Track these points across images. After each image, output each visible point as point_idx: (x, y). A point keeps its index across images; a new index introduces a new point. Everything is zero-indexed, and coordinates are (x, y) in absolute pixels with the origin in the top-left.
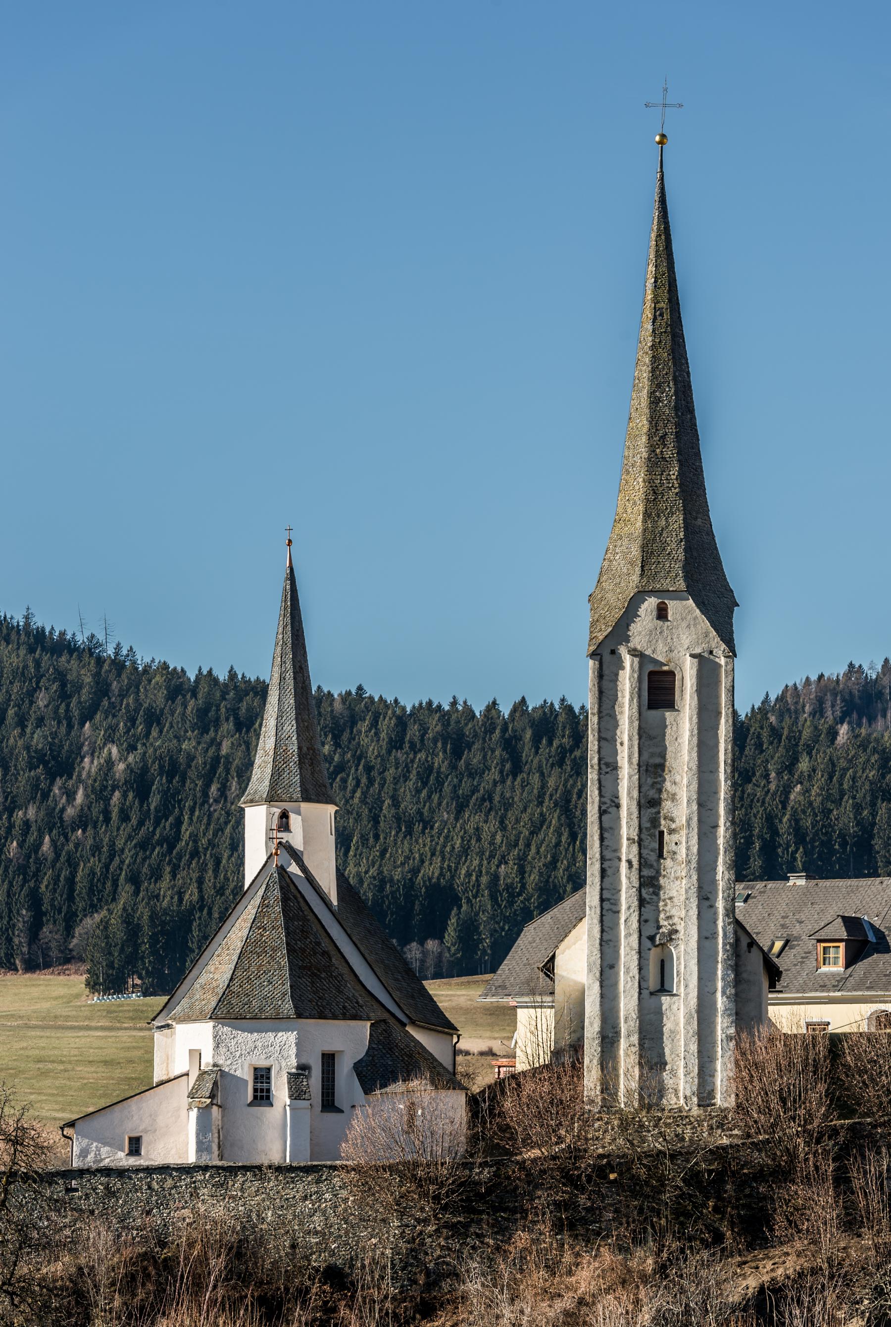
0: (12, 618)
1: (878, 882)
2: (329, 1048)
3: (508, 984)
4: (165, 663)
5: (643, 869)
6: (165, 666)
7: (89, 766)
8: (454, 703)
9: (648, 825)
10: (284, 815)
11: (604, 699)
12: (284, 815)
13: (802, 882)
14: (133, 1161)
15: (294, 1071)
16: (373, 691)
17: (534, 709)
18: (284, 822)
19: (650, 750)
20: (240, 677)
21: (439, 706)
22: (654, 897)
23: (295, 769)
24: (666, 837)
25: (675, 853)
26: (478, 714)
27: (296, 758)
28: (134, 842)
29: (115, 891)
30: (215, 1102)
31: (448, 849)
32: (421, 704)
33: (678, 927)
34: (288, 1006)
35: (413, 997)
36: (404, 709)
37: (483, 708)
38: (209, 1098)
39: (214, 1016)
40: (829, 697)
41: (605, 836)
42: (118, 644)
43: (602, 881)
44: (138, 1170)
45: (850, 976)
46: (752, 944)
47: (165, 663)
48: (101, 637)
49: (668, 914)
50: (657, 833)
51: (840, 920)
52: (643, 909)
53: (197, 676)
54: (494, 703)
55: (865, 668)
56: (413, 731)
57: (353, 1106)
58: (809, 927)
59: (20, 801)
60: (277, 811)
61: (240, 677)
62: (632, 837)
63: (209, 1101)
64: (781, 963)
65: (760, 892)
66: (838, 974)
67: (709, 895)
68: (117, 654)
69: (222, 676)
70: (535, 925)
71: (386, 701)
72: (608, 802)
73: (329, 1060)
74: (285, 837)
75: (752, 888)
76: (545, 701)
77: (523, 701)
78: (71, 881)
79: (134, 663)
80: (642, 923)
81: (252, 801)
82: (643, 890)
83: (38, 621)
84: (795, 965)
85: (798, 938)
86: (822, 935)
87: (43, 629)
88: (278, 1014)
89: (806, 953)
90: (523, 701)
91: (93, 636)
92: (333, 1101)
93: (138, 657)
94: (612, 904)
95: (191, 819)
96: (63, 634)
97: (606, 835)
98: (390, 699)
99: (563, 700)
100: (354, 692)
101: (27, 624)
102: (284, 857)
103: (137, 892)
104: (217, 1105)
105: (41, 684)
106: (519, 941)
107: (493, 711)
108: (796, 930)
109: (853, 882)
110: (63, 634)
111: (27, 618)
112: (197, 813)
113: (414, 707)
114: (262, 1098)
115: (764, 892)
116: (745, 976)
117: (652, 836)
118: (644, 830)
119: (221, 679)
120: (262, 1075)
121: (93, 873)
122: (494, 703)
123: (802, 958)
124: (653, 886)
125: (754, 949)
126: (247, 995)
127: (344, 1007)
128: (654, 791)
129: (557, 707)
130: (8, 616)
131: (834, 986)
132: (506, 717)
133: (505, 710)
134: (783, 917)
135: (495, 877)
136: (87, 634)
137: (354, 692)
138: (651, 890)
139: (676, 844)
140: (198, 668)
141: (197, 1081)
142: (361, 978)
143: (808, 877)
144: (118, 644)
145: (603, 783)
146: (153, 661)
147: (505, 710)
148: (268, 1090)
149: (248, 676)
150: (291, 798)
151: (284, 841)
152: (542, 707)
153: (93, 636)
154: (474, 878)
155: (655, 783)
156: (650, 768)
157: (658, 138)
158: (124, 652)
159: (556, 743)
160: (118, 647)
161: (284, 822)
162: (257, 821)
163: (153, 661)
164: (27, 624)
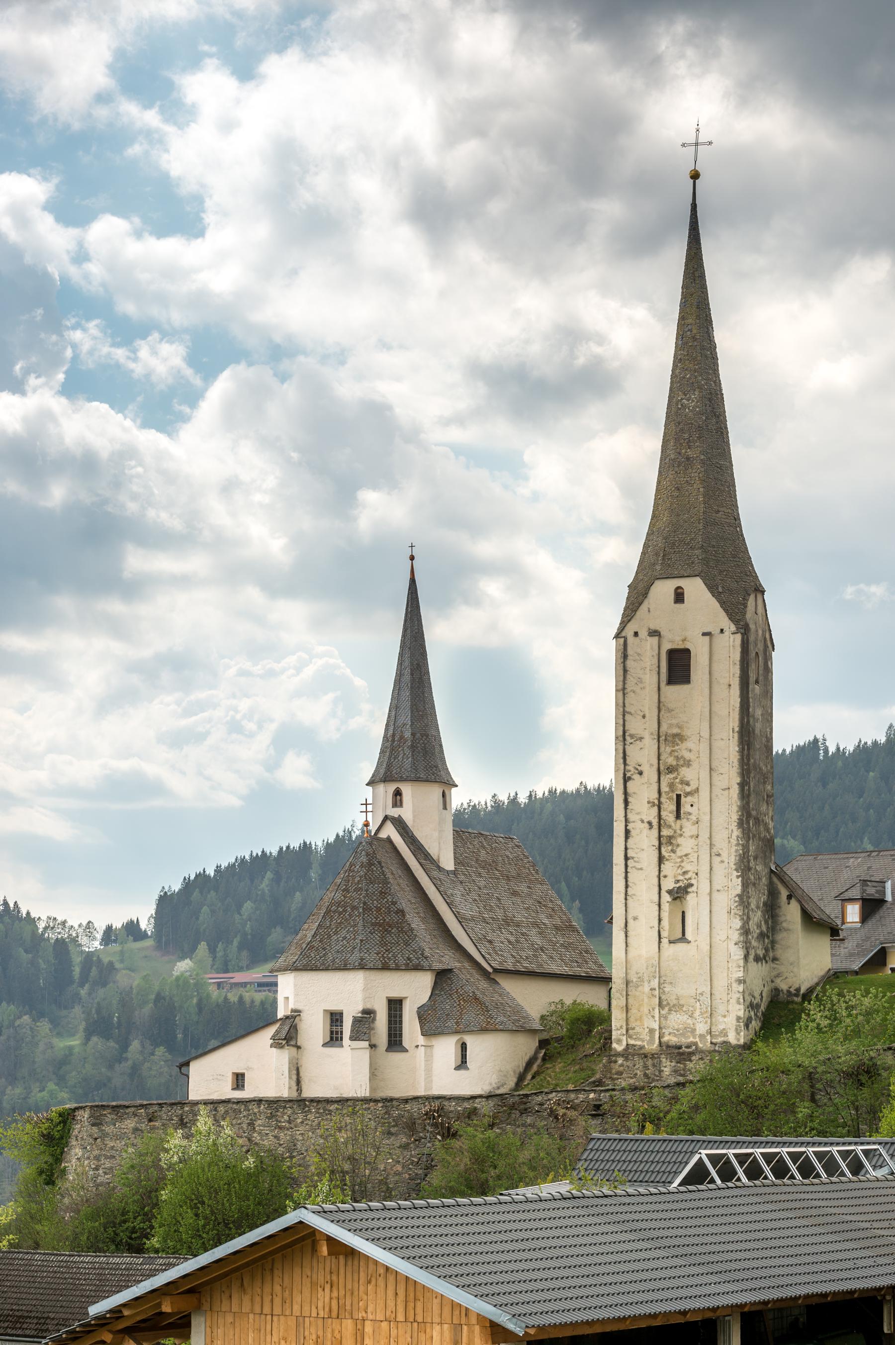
2: (395, 994)
5: (663, 830)
9: (667, 789)
10: (398, 793)
11: (628, 676)
12: (398, 793)
15: (360, 1015)
22: (672, 854)
24: (683, 799)
33: (693, 881)
38: (285, 1039)
43: (626, 841)
49: (684, 870)
50: (675, 797)
52: (662, 866)
57: (417, 1046)
59: (646, 978)
72: (632, 769)
73: (395, 1005)
80: (662, 878)
86: (847, 895)
88: (345, 965)
92: (401, 1041)
97: (630, 799)
114: (337, 1039)
117: (670, 799)
118: (663, 795)
126: (324, 949)
127: (409, 959)
139: (692, 805)
145: (628, 753)
150: (401, 777)
155: (673, 751)
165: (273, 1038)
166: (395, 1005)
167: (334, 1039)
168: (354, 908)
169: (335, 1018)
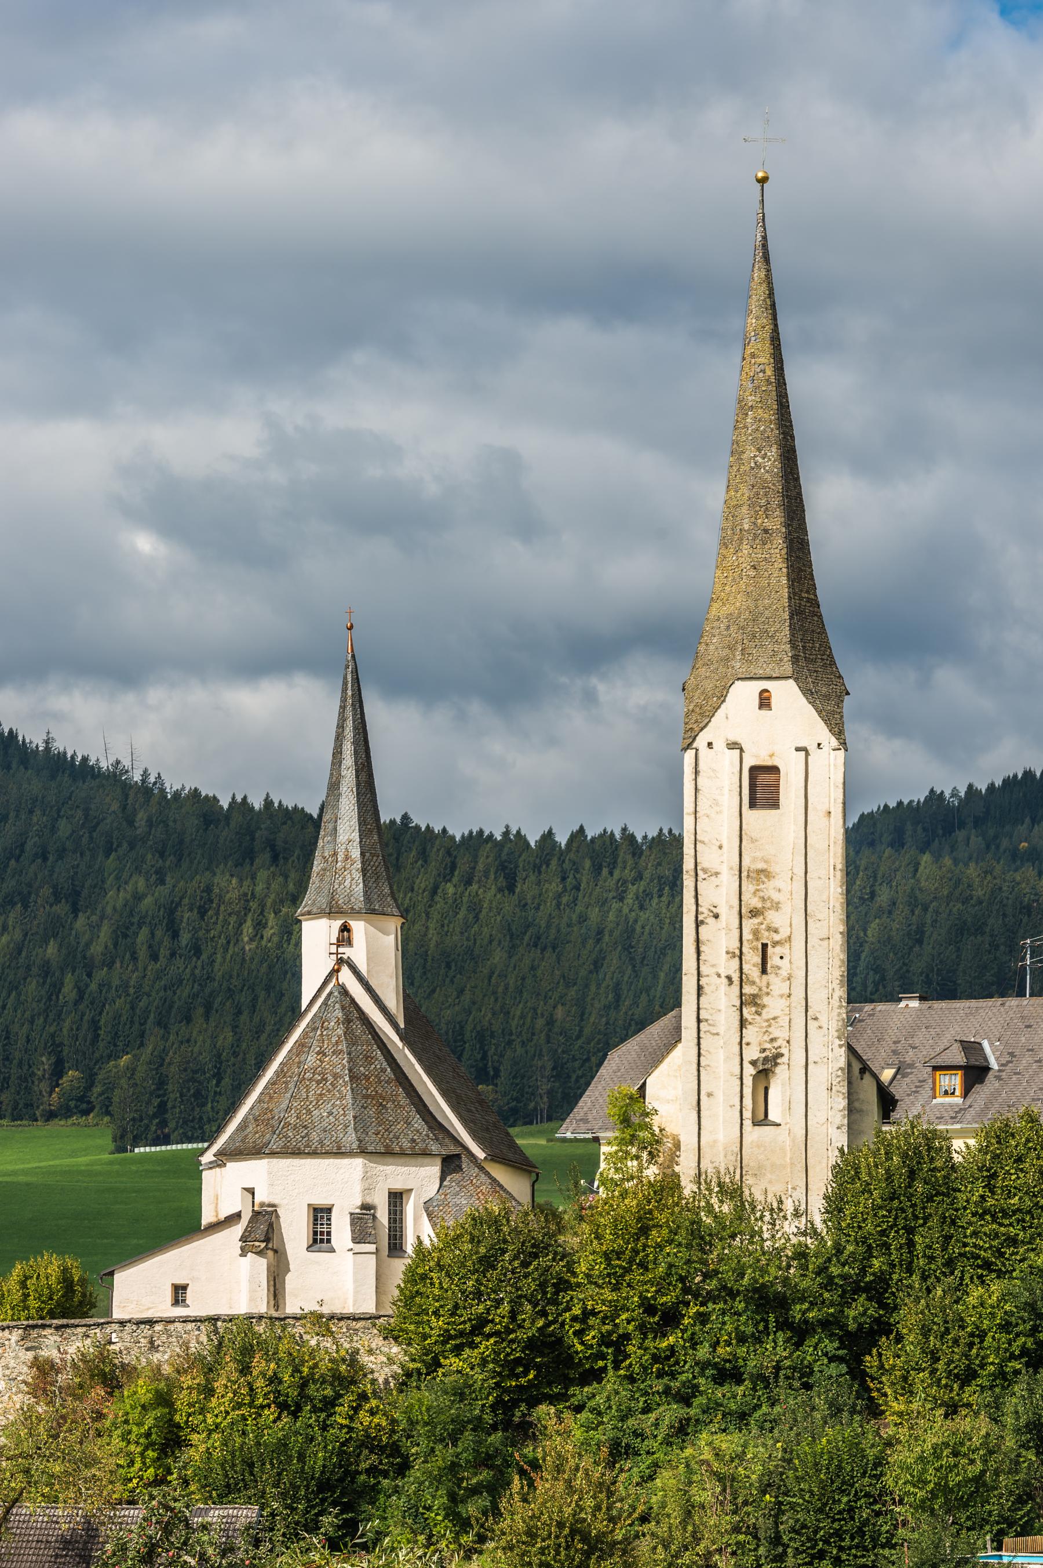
0: (31, 742)
1: (999, 1003)
3: (590, 1117)
4: (196, 789)
6: (196, 793)
7: (114, 899)
8: (506, 834)
9: (751, 937)
10: (345, 928)
12: (345, 928)
13: (915, 1004)
14: (180, 1312)
16: (420, 821)
17: (593, 839)
18: (345, 936)
19: (753, 855)
20: (276, 805)
21: (491, 836)
22: (757, 1017)
23: (358, 876)
24: (770, 950)
25: (779, 968)
26: (533, 844)
27: (358, 865)
28: (163, 983)
29: (142, 1035)
30: (270, 1246)
31: (500, 989)
32: (471, 832)
34: (350, 1139)
35: (487, 1129)
36: (453, 838)
37: (538, 838)
39: (363, 1152)
40: (909, 827)
41: (701, 949)
42: (146, 771)
44: (185, 1320)
45: (970, 1107)
46: (865, 1069)
47: (196, 789)
48: (126, 763)
49: (771, 1036)
50: (760, 946)
51: (957, 1045)
52: (744, 1030)
53: (230, 804)
54: (550, 832)
55: (947, 795)
56: (463, 865)
58: (926, 1052)
60: (338, 924)
61: (276, 805)
62: (731, 950)
63: (263, 1245)
64: (897, 1091)
65: (870, 1015)
66: (957, 1105)
67: (818, 1015)
68: (143, 781)
69: (257, 803)
70: (619, 1052)
71: (433, 831)
73: (397, 1198)
74: (347, 952)
75: (860, 1011)
76: (605, 830)
77: (582, 829)
78: (95, 1025)
79: (162, 790)
81: (309, 913)
82: (744, 1009)
83: (58, 746)
84: (909, 1095)
85: (911, 1066)
86: (939, 1061)
87: (65, 753)
89: (920, 1081)
90: (582, 829)
91: (118, 762)
93: (167, 785)
94: (710, 1025)
95: (224, 958)
96: (85, 759)
98: (437, 829)
99: (624, 830)
100: (398, 821)
101: (47, 749)
102: (346, 976)
103: (165, 1038)
104: (272, 1249)
105: (62, 813)
106: (602, 1071)
107: (549, 841)
108: (910, 1056)
109: (973, 1003)
110: (85, 759)
111: (47, 742)
112: (230, 952)
113: (463, 836)
115: (873, 1015)
116: (857, 1105)
119: (257, 807)
120: (320, 1214)
121: (117, 1016)
122: (550, 832)
123: (916, 1087)
124: (756, 1004)
125: (867, 1076)
128: (756, 899)
129: (618, 836)
130: (27, 741)
131: (952, 1118)
132: (563, 846)
133: (562, 838)
134: (895, 1043)
135: (551, 1022)
136: (112, 760)
137: (398, 821)
138: (754, 1009)
140: (231, 795)
141: (249, 1222)
142: (431, 1108)
143: (922, 999)
144: (146, 771)
146: (183, 788)
147: (562, 838)
148: (329, 1233)
149: (285, 803)
151: (345, 957)
152: (601, 836)
153: (118, 762)
154: (529, 1020)
155: (758, 890)
156: (751, 874)
157: (760, 175)
158: (152, 779)
159: (617, 873)
160: (145, 774)
161: (345, 936)
162: (316, 938)
163: (183, 788)
164: (47, 749)
165: (244, 1239)
166: (397, 1198)
167: (320, 1239)
168: (336, 1076)
169: (320, 1214)
